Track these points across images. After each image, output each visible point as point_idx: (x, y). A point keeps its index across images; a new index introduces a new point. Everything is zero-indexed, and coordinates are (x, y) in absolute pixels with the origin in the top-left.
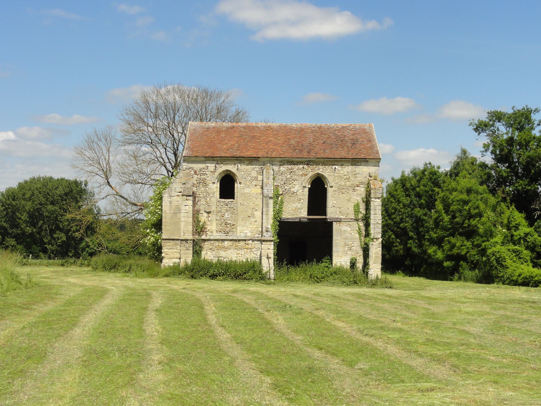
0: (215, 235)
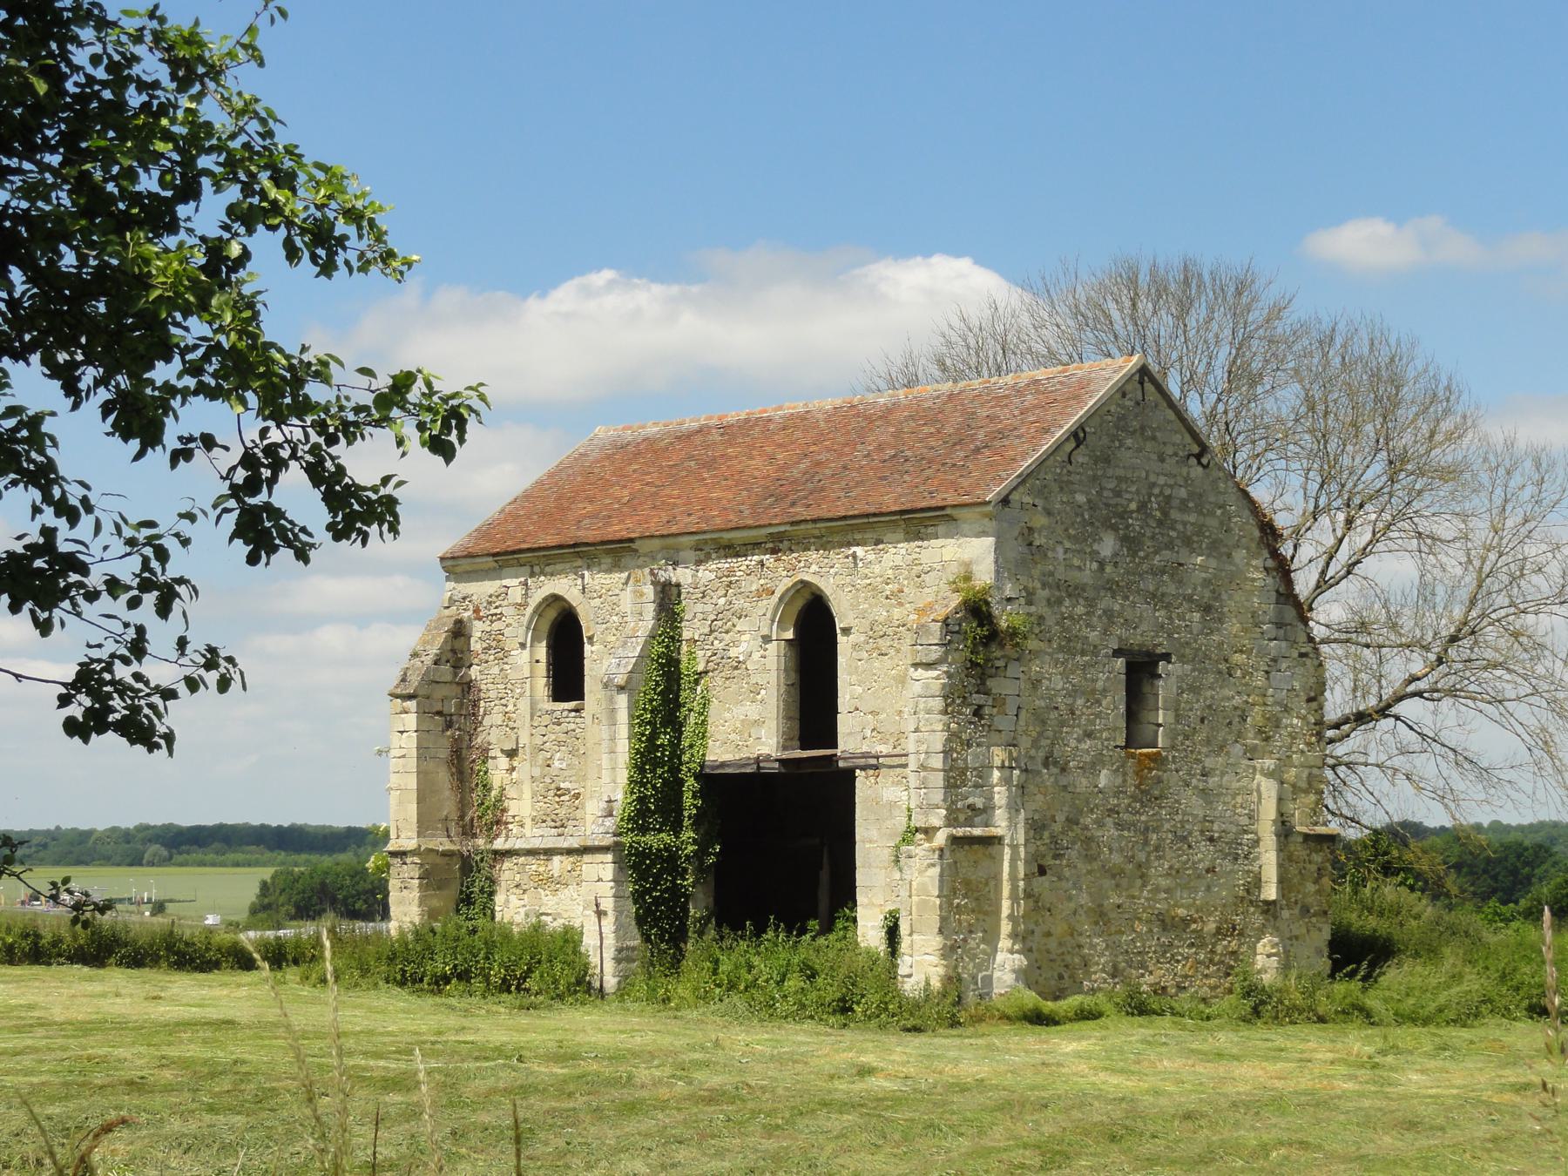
0: (528, 834)
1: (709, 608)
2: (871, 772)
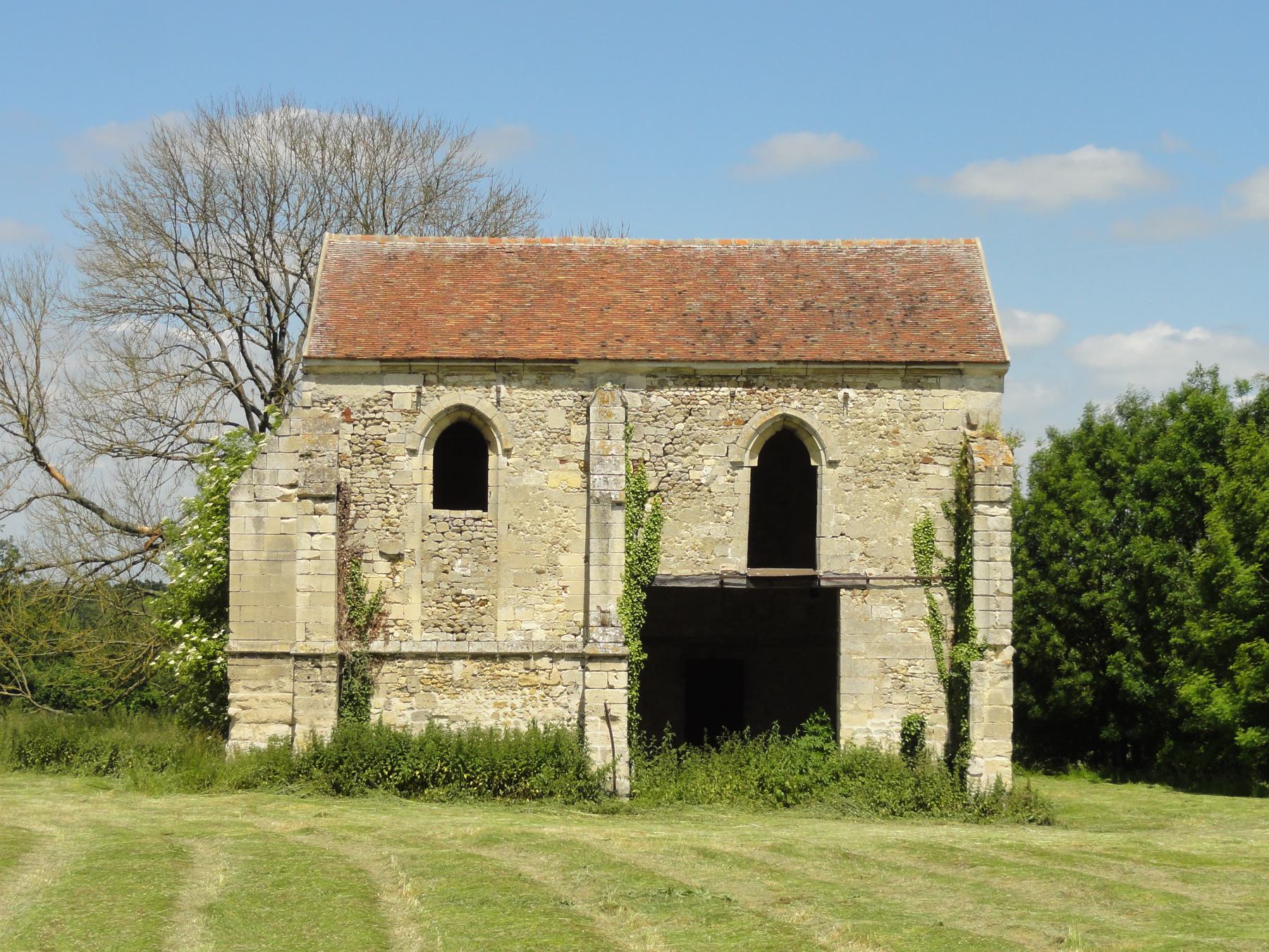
1: (665, 432)
2: (859, 592)
